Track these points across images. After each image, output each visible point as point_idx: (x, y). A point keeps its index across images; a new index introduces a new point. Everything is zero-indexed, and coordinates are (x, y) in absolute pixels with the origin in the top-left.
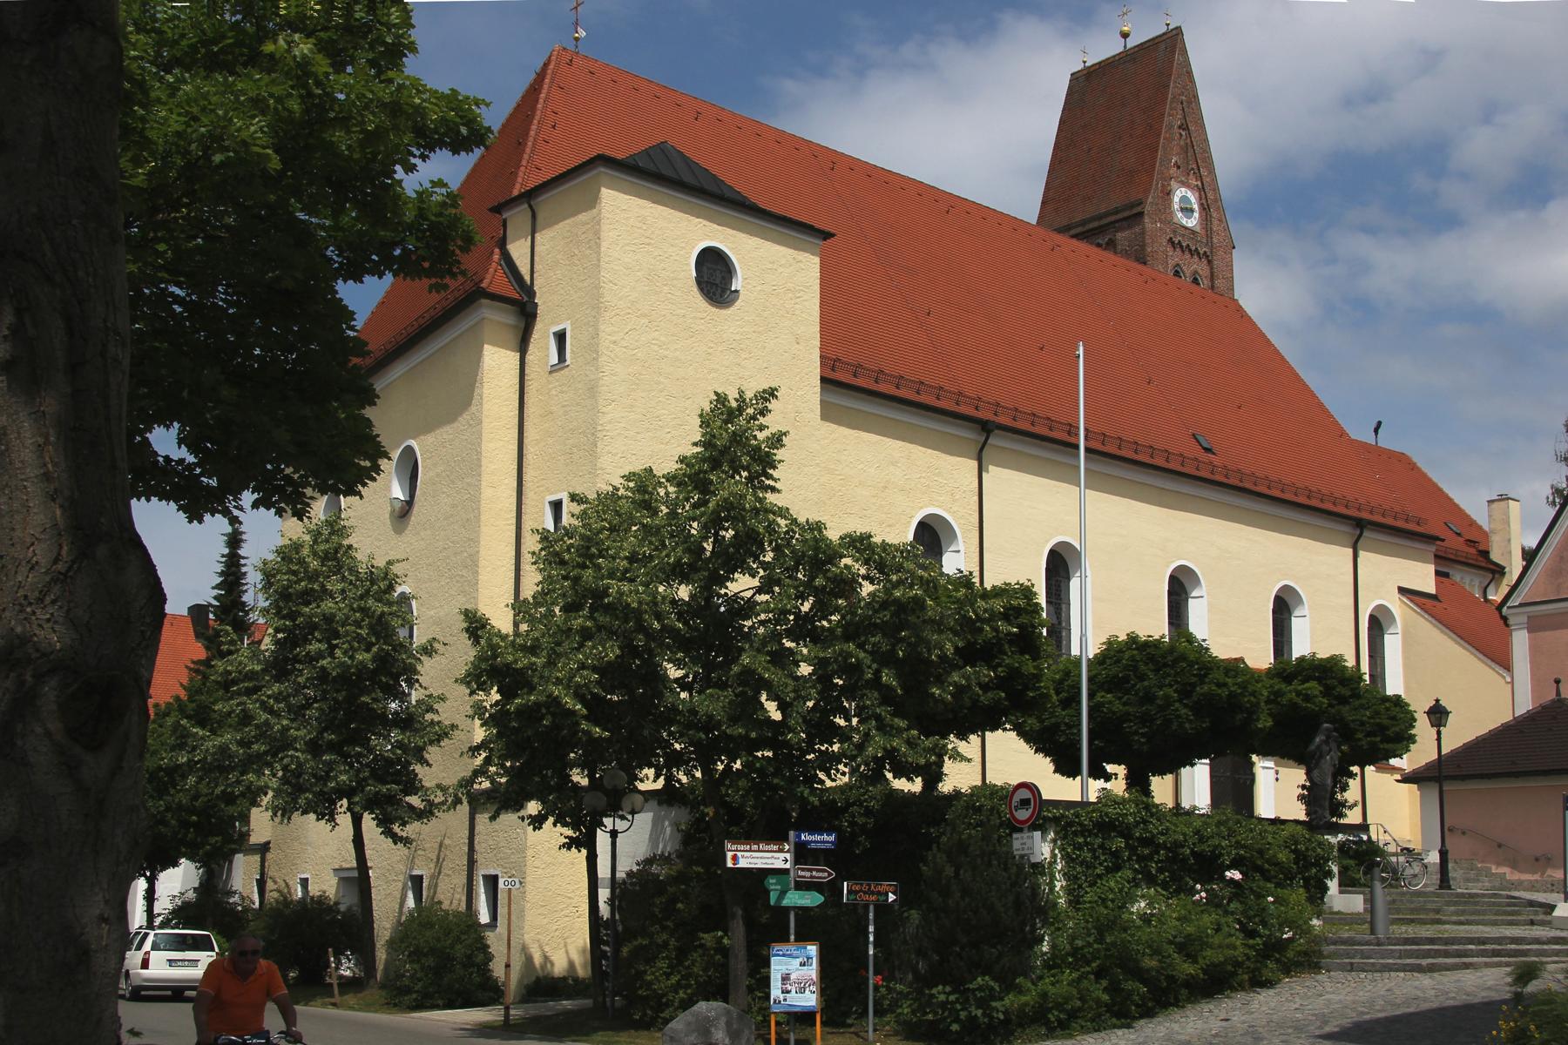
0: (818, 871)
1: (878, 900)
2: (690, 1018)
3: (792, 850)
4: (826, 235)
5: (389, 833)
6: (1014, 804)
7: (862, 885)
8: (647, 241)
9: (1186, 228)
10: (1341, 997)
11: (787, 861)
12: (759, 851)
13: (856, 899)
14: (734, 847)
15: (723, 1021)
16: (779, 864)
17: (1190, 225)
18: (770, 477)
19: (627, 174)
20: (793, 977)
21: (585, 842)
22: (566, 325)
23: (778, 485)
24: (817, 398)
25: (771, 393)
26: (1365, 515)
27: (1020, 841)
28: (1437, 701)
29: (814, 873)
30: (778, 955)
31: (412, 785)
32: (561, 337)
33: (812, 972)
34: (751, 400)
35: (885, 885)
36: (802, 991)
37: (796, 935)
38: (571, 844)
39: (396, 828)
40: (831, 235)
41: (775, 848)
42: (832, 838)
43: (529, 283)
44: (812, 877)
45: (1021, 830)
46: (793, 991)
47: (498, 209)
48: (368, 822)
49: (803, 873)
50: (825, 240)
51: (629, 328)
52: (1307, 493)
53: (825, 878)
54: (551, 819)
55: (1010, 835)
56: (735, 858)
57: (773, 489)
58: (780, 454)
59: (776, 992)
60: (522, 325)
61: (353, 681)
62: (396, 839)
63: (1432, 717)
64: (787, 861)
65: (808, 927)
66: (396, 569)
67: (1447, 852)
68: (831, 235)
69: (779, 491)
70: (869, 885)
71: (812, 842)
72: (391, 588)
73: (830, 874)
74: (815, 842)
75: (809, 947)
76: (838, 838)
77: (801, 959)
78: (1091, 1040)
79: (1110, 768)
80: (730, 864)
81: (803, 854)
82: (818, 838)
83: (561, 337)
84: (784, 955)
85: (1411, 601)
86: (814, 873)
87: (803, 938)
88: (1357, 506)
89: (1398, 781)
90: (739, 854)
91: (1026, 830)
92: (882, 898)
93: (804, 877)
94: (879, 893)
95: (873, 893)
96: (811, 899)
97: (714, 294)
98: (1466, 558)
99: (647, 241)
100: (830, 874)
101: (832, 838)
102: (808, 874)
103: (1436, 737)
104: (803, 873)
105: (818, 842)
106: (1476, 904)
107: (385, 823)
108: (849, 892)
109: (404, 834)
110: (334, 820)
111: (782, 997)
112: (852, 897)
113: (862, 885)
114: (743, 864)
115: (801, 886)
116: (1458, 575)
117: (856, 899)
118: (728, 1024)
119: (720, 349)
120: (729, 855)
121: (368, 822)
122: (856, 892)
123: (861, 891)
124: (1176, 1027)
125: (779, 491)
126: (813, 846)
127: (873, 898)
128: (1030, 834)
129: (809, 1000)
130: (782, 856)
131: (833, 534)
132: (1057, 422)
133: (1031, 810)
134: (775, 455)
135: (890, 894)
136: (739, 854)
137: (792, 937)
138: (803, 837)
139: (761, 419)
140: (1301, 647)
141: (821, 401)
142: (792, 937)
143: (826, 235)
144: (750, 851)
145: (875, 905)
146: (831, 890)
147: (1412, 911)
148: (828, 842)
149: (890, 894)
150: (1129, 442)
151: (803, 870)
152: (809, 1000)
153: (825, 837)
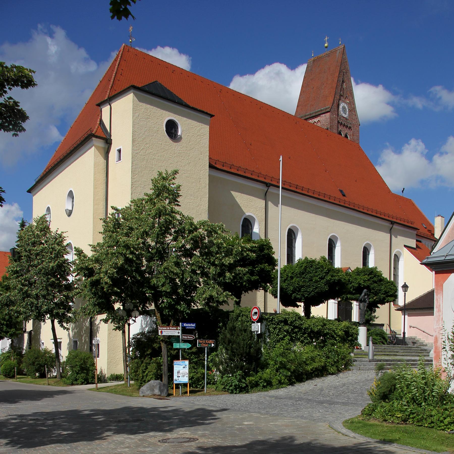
0: (189, 336)
1: (208, 346)
2: (148, 386)
3: (181, 329)
4: (212, 116)
5: (62, 326)
6: (253, 314)
7: (203, 341)
8: (149, 117)
9: (344, 117)
10: (353, 378)
11: (179, 333)
12: (170, 329)
13: (201, 346)
14: (161, 328)
15: (158, 386)
16: (176, 334)
17: (345, 116)
18: (177, 201)
19: (146, 94)
20: (181, 372)
21: (121, 328)
22: (121, 147)
23: (179, 204)
24: (207, 174)
25: (176, 172)
26: (394, 220)
27: (254, 326)
28: (405, 283)
29: (188, 337)
30: (176, 365)
31: (69, 309)
32: (119, 151)
33: (187, 370)
34: (170, 174)
35: (211, 341)
36: (183, 376)
37: (182, 358)
38: (118, 328)
39: (65, 324)
40: (214, 116)
41: (175, 328)
42: (194, 325)
43: (109, 131)
44: (187, 338)
45: (254, 323)
46: (181, 377)
47: (99, 105)
48: (56, 321)
49: (184, 337)
50: (211, 117)
51: (142, 148)
52: (376, 211)
53: (192, 339)
54: (110, 321)
55: (251, 324)
56: (161, 332)
57: (178, 205)
58: (181, 193)
59: (175, 377)
60: (107, 147)
61: (52, 273)
62: (65, 328)
63: (403, 288)
64: (179, 333)
65: (186, 355)
66: (64, 235)
67: (405, 333)
68: (214, 116)
69: (180, 206)
70: (206, 341)
71: (187, 326)
72: (62, 241)
73: (193, 337)
74: (188, 326)
75: (186, 362)
76: (196, 325)
77: (183, 366)
78: (273, 392)
79: (298, 304)
80: (160, 334)
81: (185, 331)
82: (190, 325)
83: (119, 151)
84: (178, 365)
85: (408, 250)
86: (188, 337)
87: (184, 358)
88: (384, 214)
89: (395, 310)
90: (163, 331)
91: (256, 322)
92: (210, 345)
93: (185, 338)
94: (209, 344)
95: (207, 344)
96: (187, 346)
97: (172, 136)
98: (421, 234)
99: (149, 117)
100: (193, 337)
101: (194, 325)
102: (186, 337)
103: (404, 295)
104: (184, 337)
105: (189, 326)
106: (411, 350)
107: (60, 322)
108: (199, 343)
109: (67, 327)
110: (45, 322)
111: (177, 378)
112: (200, 345)
113: (203, 341)
114: (164, 334)
115: (185, 341)
116: (424, 241)
117: (201, 346)
118: (160, 387)
119: (174, 156)
120: (160, 331)
121: (56, 321)
122: (201, 343)
123: (203, 343)
124: (300, 387)
125: (180, 206)
126: (188, 328)
127: (207, 345)
128: (257, 324)
129: (185, 379)
130: (177, 331)
131: (195, 222)
132: (293, 184)
133: (257, 316)
134: (179, 193)
135: (212, 344)
136: (163, 331)
137: (181, 359)
138: (184, 325)
139: (173, 180)
140: (371, 264)
141: (209, 175)
142: (181, 359)
143: (212, 116)
144: (167, 329)
145: (207, 348)
146: (193, 343)
147: (390, 352)
148: (193, 326)
149: (212, 344)
150: (317, 192)
151: (184, 336)
152: (185, 379)
153: (192, 325)
